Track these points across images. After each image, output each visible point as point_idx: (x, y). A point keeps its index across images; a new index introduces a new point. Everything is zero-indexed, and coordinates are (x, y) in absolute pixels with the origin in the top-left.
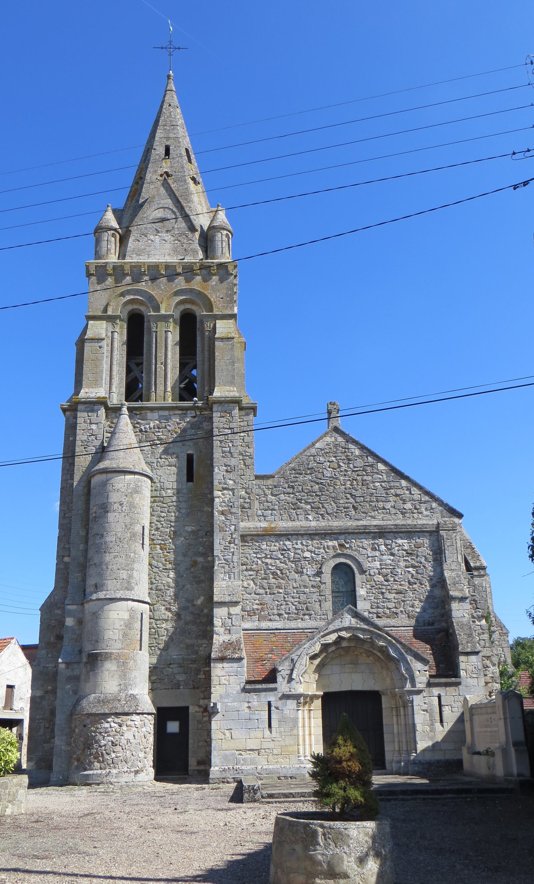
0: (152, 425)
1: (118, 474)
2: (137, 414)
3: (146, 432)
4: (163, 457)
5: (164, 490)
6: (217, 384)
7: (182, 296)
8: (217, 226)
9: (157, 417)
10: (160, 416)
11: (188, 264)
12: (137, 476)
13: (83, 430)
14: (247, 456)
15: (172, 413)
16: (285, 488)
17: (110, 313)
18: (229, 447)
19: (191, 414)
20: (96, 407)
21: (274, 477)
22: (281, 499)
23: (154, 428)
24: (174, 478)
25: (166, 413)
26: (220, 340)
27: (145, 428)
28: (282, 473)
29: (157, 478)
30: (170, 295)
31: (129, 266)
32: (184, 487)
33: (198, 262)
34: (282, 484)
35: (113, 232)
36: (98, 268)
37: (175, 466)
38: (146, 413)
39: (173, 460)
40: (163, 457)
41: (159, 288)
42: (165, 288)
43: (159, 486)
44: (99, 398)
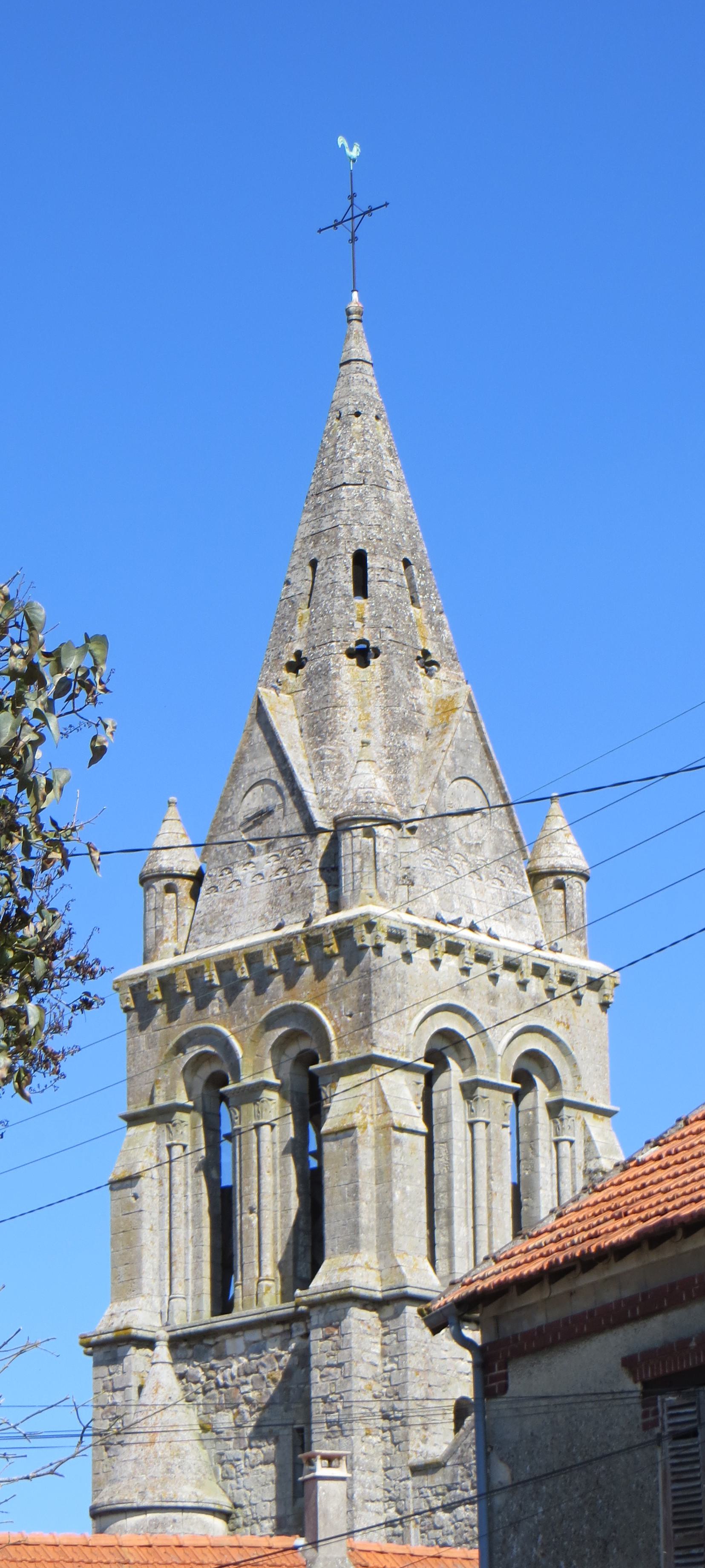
0: (236, 1366)
1: (114, 1517)
2: (211, 1346)
3: (226, 1386)
4: (253, 1444)
5: (258, 1523)
6: (328, 1251)
7: (280, 1027)
8: (343, 815)
9: (242, 1348)
10: (248, 1344)
11: (282, 943)
12: (150, 1516)
13: (103, 1407)
14: (396, 1419)
15: (267, 1332)
16: (466, 1490)
17: (160, 1102)
18: (338, 1411)
19: (298, 1329)
20: (120, 1350)
21: (445, 1466)
22: (459, 1518)
23: (239, 1376)
24: (270, 1492)
25: (255, 1335)
26: (333, 1136)
27: (224, 1378)
28: (459, 1452)
29: (246, 1496)
30: (256, 1031)
31: (184, 973)
32: (289, 1512)
33: (301, 933)
34: (459, 1480)
35: (165, 881)
36: (137, 988)
37: (273, 1462)
38: (224, 1341)
39: (269, 1448)
40: (253, 1444)
41: (242, 1015)
42: (252, 1013)
43: (249, 1513)
44: (117, 1330)
